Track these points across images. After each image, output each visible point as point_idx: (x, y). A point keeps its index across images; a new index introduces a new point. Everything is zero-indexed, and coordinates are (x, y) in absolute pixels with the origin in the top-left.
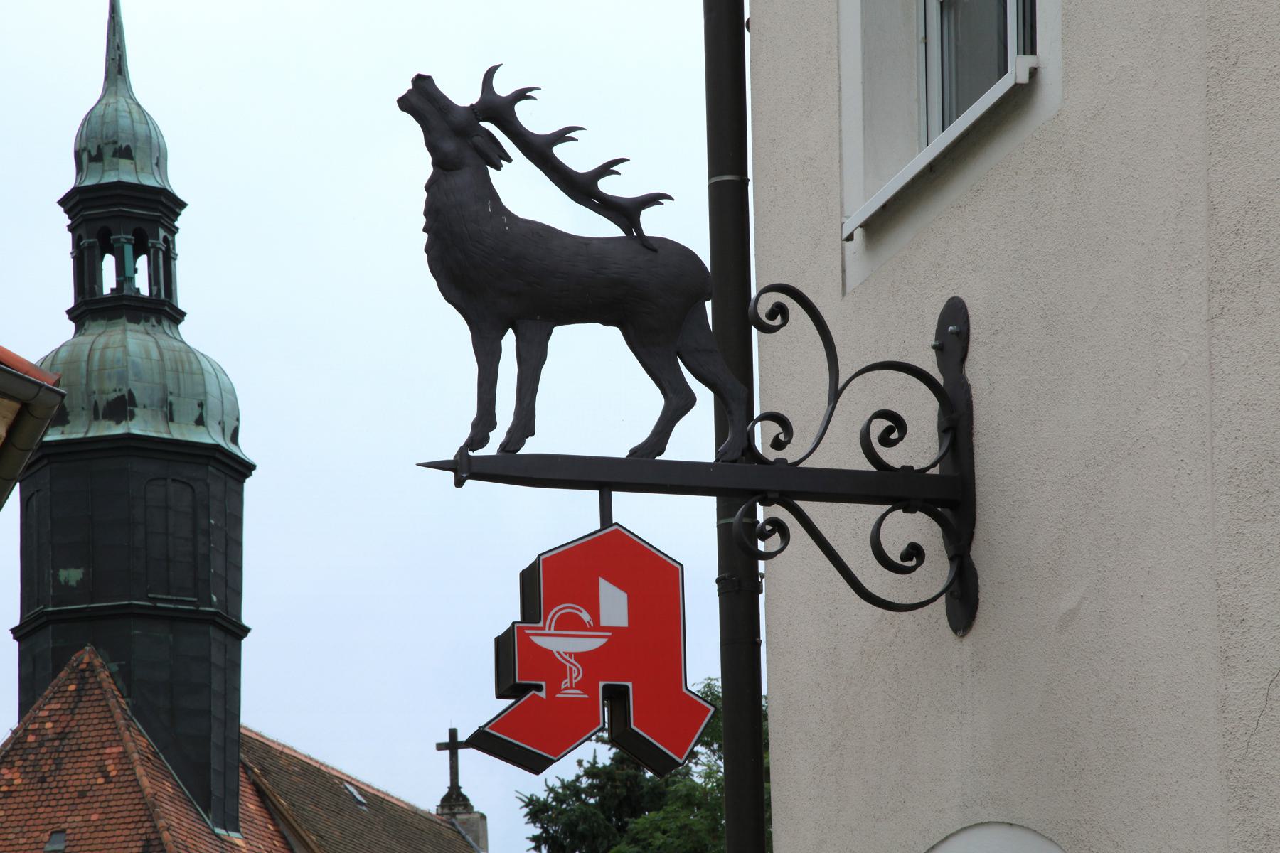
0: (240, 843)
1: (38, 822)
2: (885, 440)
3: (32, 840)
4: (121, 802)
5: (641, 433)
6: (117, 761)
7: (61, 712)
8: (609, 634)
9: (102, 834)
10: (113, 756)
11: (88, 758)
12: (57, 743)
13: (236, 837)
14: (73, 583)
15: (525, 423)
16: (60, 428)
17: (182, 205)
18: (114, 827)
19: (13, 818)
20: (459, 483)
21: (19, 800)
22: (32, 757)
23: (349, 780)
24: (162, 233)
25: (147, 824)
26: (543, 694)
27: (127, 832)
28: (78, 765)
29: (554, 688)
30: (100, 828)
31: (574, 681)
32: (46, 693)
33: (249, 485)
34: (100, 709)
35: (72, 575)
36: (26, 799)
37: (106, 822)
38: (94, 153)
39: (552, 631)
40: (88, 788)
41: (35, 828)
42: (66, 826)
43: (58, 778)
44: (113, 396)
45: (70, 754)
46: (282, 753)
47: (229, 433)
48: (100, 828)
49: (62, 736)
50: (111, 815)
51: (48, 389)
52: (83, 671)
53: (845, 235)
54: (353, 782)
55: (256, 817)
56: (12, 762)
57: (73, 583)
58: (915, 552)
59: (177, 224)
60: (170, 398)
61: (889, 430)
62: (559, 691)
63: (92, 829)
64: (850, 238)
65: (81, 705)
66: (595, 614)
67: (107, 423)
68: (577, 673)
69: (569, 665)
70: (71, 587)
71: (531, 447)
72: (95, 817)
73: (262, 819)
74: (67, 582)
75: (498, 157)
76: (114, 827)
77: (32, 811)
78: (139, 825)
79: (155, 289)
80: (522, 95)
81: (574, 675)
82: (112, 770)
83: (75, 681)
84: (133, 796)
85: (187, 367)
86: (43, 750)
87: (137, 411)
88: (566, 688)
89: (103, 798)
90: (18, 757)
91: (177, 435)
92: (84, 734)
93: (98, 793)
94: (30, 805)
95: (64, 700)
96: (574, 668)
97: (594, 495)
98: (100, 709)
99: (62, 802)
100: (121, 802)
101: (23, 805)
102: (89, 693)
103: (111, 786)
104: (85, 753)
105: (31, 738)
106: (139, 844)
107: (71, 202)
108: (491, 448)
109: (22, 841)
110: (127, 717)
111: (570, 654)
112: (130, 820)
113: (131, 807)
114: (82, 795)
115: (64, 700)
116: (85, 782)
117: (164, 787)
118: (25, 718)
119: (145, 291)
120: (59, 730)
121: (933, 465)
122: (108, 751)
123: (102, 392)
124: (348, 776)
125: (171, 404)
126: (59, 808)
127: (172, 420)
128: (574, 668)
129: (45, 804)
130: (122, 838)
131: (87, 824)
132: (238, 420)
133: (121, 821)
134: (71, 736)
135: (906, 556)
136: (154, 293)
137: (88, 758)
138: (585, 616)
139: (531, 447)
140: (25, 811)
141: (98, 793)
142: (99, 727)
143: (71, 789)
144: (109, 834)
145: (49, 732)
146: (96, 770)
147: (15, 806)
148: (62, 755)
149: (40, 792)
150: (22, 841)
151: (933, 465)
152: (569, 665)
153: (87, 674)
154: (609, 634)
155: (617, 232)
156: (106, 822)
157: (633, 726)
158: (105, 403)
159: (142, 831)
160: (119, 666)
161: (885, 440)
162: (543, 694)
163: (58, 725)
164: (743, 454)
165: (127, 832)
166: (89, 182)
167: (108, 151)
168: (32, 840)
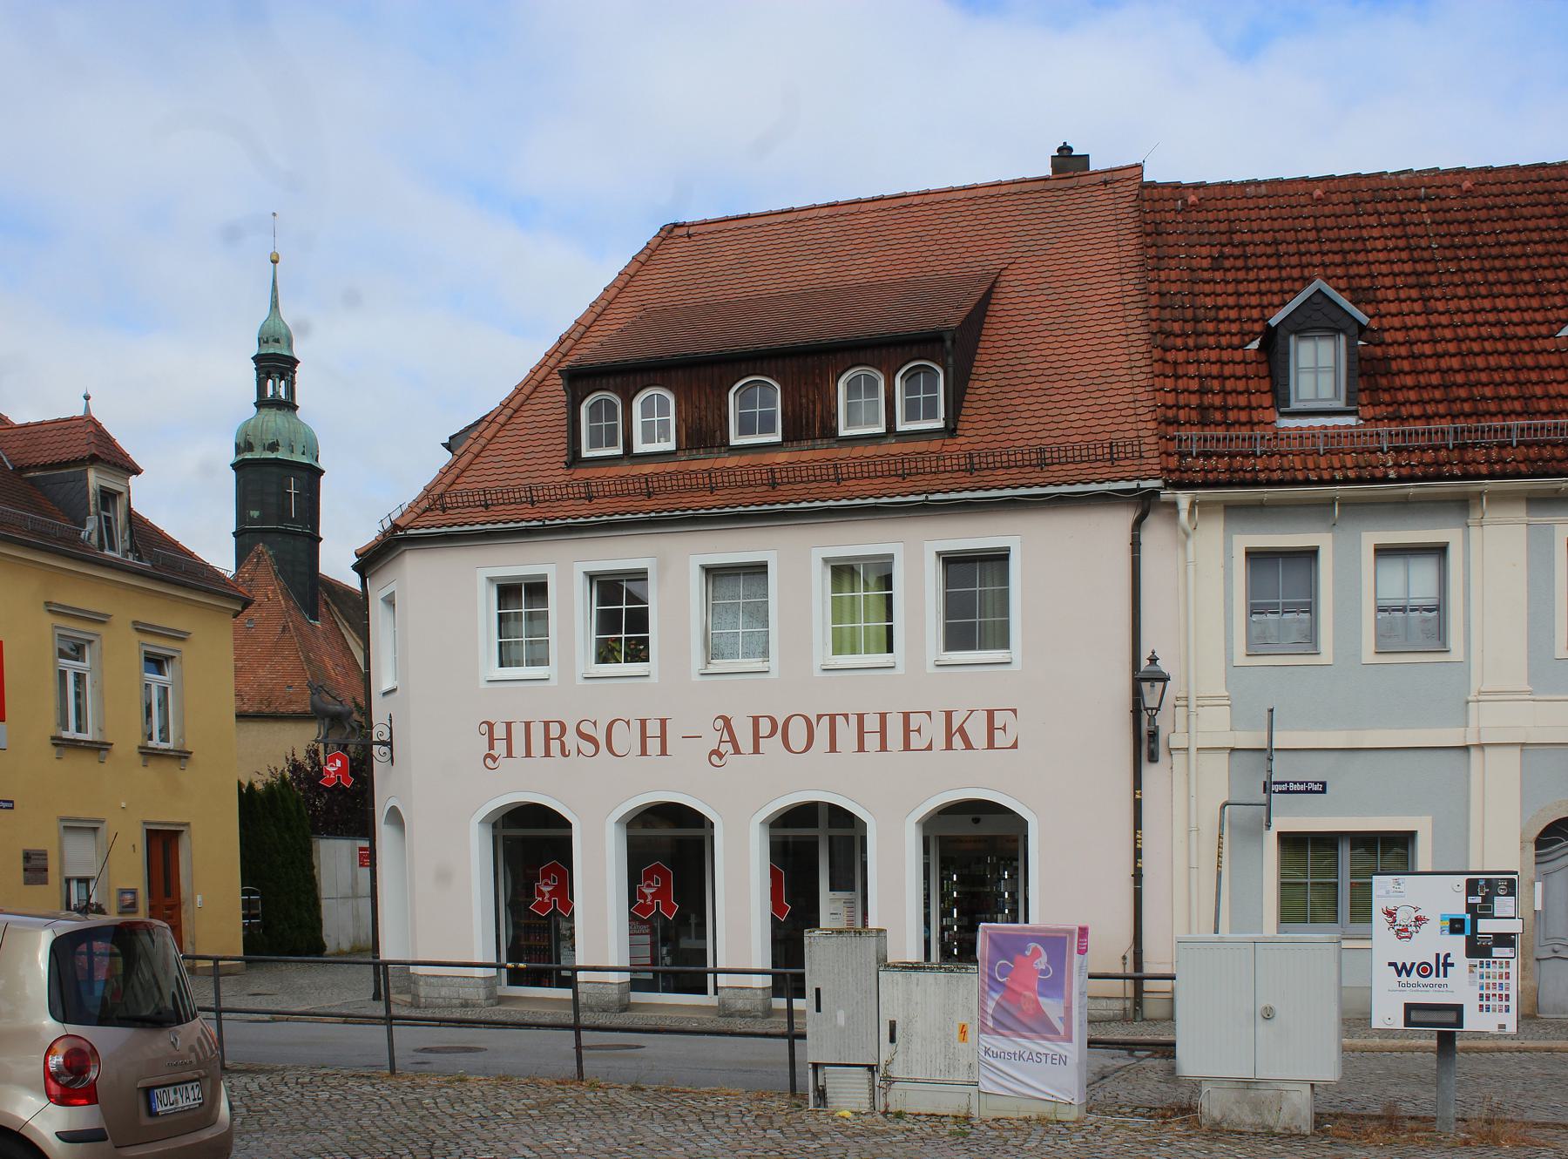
13: (318, 624)
35: (255, 514)
49: (252, 580)
167: (271, 340)
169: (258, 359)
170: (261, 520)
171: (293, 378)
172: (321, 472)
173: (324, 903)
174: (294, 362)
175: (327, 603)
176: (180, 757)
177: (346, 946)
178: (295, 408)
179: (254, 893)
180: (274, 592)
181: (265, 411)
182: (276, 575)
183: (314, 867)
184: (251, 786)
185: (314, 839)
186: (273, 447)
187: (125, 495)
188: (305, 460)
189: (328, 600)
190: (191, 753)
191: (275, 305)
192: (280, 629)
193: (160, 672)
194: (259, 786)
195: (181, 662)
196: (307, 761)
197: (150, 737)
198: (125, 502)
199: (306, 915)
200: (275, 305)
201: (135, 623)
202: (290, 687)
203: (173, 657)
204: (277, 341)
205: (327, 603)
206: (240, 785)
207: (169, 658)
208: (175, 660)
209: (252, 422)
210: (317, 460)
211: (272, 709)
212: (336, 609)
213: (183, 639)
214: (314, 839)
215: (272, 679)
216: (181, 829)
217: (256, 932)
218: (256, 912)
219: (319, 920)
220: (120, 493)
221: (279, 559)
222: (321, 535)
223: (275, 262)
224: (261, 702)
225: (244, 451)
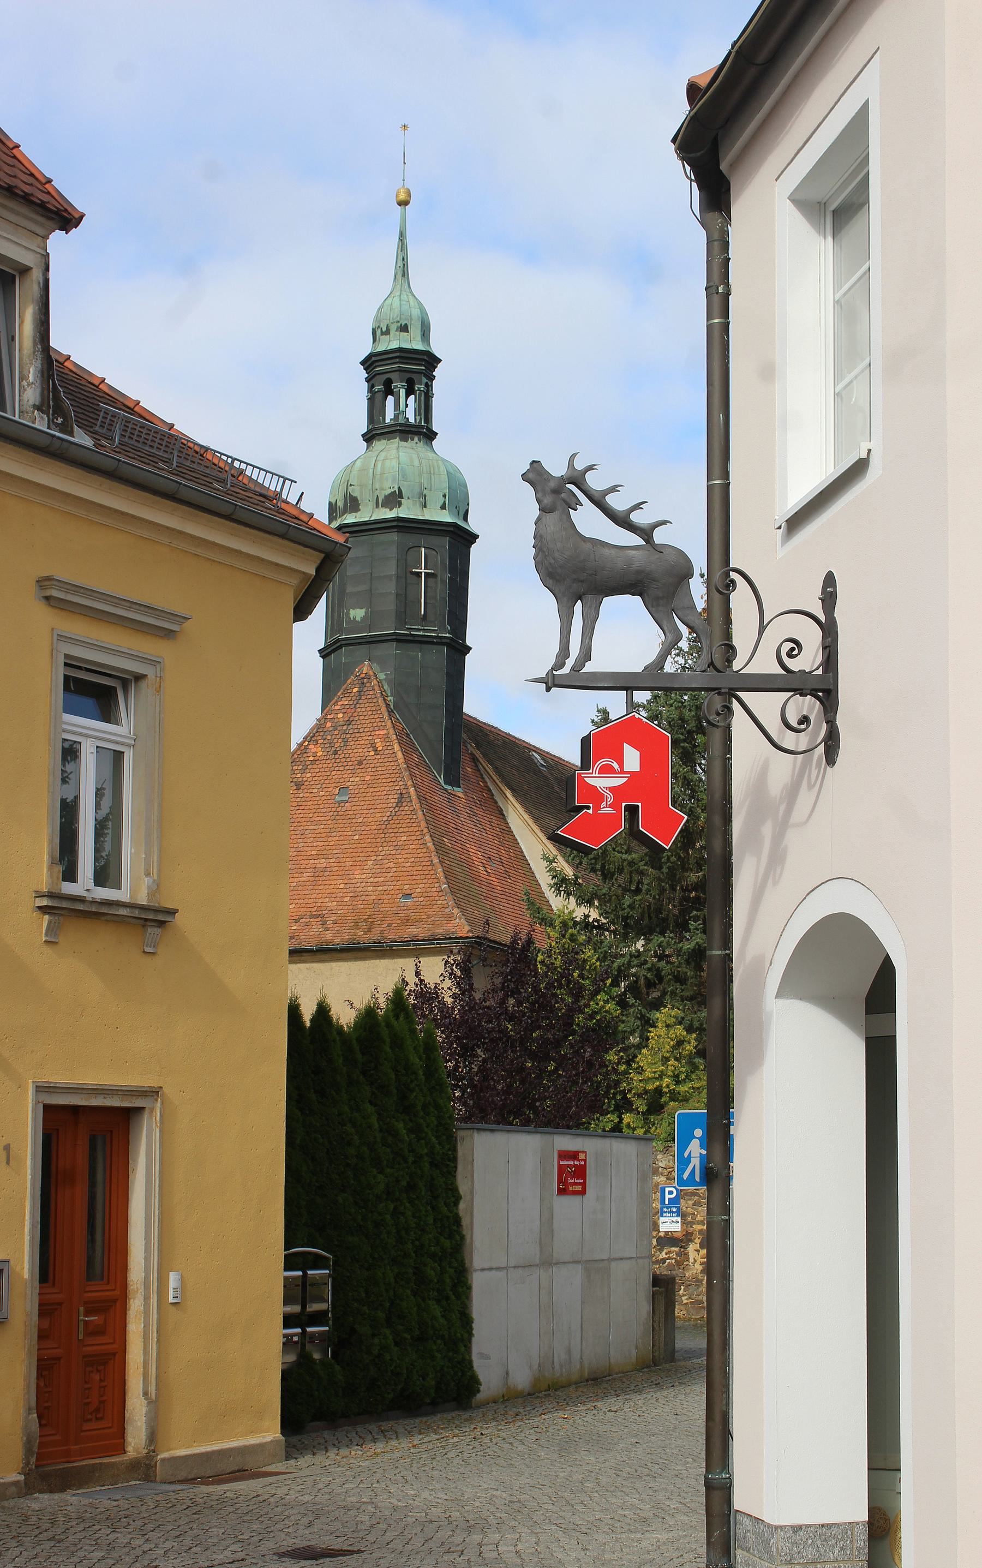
0: (461, 795)
1: (333, 781)
2: (790, 655)
3: (328, 793)
4: (385, 768)
5: (651, 656)
6: (382, 740)
7: (348, 707)
8: (629, 775)
9: (372, 790)
10: (380, 736)
11: (364, 738)
12: (345, 728)
13: (458, 791)
14: (358, 619)
15: (586, 655)
16: (354, 514)
17: (439, 361)
18: (379, 785)
19: (316, 778)
20: (548, 689)
21: (320, 766)
22: (329, 737)
23: (535, 749)
24: (424, 380)
25: (401, 783)
26: (590, 811)
27: (387, 788)
28: (358, 743)
29: (597, 807)
30: (370, 786)
31: (608, 803)
32: (339, 694)
33: (474, 549)
34: (373, 704)
35: (358, 614)
36: (325, 766)
37: (375, 781)
38: (384, 329)
39: (597, 775)
40: (364, 758)
41: (330, 785)
42: (350, 783)
43: (345, 752)
44: (389, 491)
45: (353, 736)
46: (490, 731)
47: (462, 513)
48: (370, 786)
49: (349, 723)
50: (378, 777)
51: (341, 544)
52: (363, 678)
53: (777, 526)
54: (538, 751)
55: (472, 776)
56: (317, 741)
57: (358, 619)
58: (805, 720)
59: (434, 373)
60: (425, 492)
61: (793, 649)
62: (600, 809)
63: (366, 786)
64: (780, 528)
65: (361, 701)
66: (621, 764)
67: (384, 510)
68: (610, 798)
69: (605, 794)
70: (357, 622)
71: (589, 668)
72: (367, 778)
73: (476, 778)
74: (354, 618)
75: (574, 504)
76: (379, 785)
77: (328, 773)
78: (396, 783)
79: (418, 418)
80: (590, 468)
81: (608, 800)
82: (379, 746)
83: (358, 686)
84: (392, 763)
85: (436, 470)
86: (336, 732)
87: (403, 501)
88: (604, 807)
89: (373, 765)
90: (320, 737)
91: (428, 517)
92: (363, 722)
93: (370, 762)
94: (326, 770)
95: (350, 698)
96: (608, 796)
97: (623, 693)
98: (373, 704)
99: (347, 768)
100: (385, 768)
101: (323, 770)
102: (366, 693)
103: (379, 757)
104: (363, 734)
105: (329, 724)
106: (396, 796)
107: (369, 363)
108: (566, 670)
109: (321, 794)
110: (390, 710)
111: (607, 788)
112: (390, 780)
113: (390, 772)
114: (360, 763)
115: (350, 698)
116: (362, 754)
117: (412, 757)
118: (325, 711)
119: (412, 420)
120: (347, 719)
121: (817, 669)
122: (377, 733)
123: (382, 489)
124: (534, 747)
125: (425, 496)
126: (345, 772)
127: (425, 506)
128: (608, 796)
129: (336, 769)
130: (385, 793)
131: (363, 783)
132: (468, 504)
133: (384, 781)
134: (353, 723)
135: (800, 723)
136: (418, 421)
137: (364, 738)
138: (616, 766)
139: (589, 668)
140: (324, 774)
141: (370, 762)
142: (372, 717)
143: (353, 759)
144: (377, 790)
145: (341, 720)
146: (369, 746)
147: (318, 770)
148: (348, 736)
149: (333, 761)
150: (321, 794)
151: (817, 669)
152: (605, 794)
153: (365, 681)
154: (629, 775)
155: (640, 541)
156: (375, 781)
157: (641, 829)
158: (383, 497)
159: (397, 788)
160: (385, 674)
161: (790, 655)
162: (590, 811)
163: (346, 715)
164: (709, 667)
165: (387, 788)
166: (381, 348)
167: (393, 328)
168: (328, 793)
169: (369, 363)
170: (370, 621)
171: (429, 387)
172: (473, 538)
173: (478, 1281)
174: (431, 361)
175: (474, 759)
176: (145, 923)
177: (522, 1379)
178: (430, 436)
179: (317, 1262)
180: (386, 738)
181: (379, 445)
182: (390, 712)
183: (458, 1198)
184: (323, 1011)
185: (461, 1134)
186: (394, 499)
187: (36, 274)
188: (446, 517)
189: (478, 754)
190: (172, 912)
191: (403, 271)
192: (393, 799)
193: (107, 713)
194: (345, 1016)
195: (158, 690)
196: (448, 983)
197: (70, 875)
198: (35, 290)
199: (437, 1310)
200: (403, 271)
201: (44, 582)
202: (407, 896)
203: (139, 678)
204: (404, 329)
205: (474, 759)
206: (294, 1012)
207: (130, 680)
208: (143, 684)
209: (358, 464)
210: (465, 518)
211: (375, 935)
212: (489, 768)
213: (169, 634)
214: (461, 1134)
215: (377, 885)
216: (138, 1103)
217: (316, 1356)
218: (321, 1306)
219: (466, 1321)
220: (24, 271)
221: (398, 686)
222: (468, 643)
223: (404, 203)
224: (356, 925)
225: (344, 512)
